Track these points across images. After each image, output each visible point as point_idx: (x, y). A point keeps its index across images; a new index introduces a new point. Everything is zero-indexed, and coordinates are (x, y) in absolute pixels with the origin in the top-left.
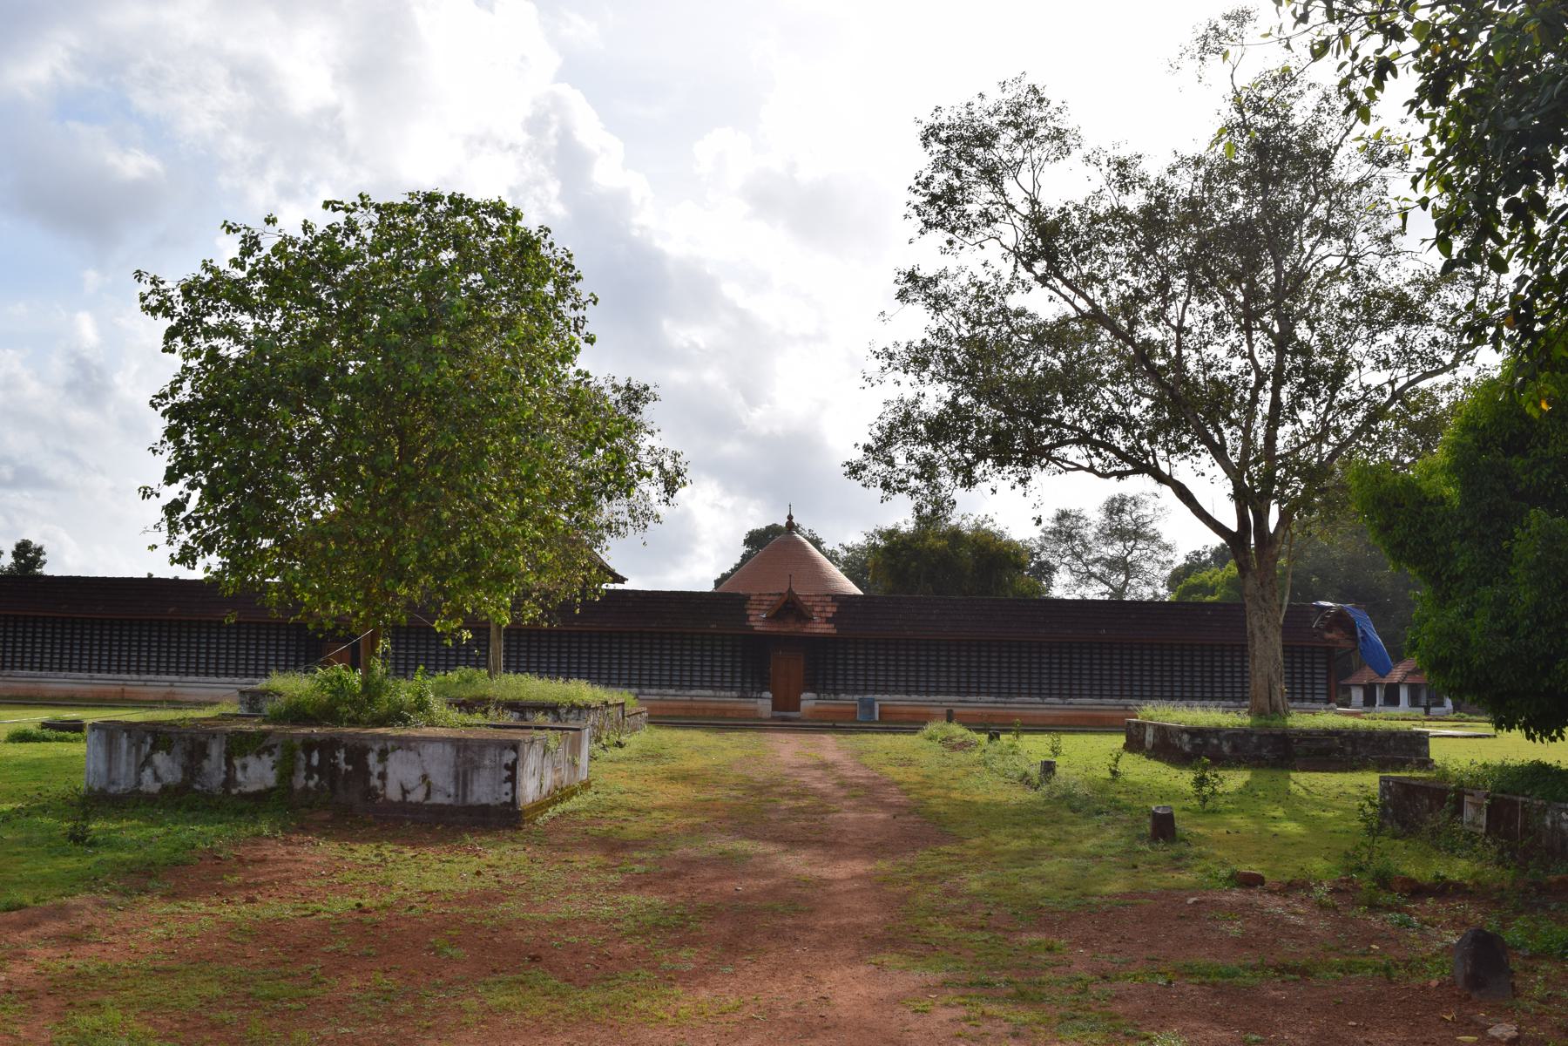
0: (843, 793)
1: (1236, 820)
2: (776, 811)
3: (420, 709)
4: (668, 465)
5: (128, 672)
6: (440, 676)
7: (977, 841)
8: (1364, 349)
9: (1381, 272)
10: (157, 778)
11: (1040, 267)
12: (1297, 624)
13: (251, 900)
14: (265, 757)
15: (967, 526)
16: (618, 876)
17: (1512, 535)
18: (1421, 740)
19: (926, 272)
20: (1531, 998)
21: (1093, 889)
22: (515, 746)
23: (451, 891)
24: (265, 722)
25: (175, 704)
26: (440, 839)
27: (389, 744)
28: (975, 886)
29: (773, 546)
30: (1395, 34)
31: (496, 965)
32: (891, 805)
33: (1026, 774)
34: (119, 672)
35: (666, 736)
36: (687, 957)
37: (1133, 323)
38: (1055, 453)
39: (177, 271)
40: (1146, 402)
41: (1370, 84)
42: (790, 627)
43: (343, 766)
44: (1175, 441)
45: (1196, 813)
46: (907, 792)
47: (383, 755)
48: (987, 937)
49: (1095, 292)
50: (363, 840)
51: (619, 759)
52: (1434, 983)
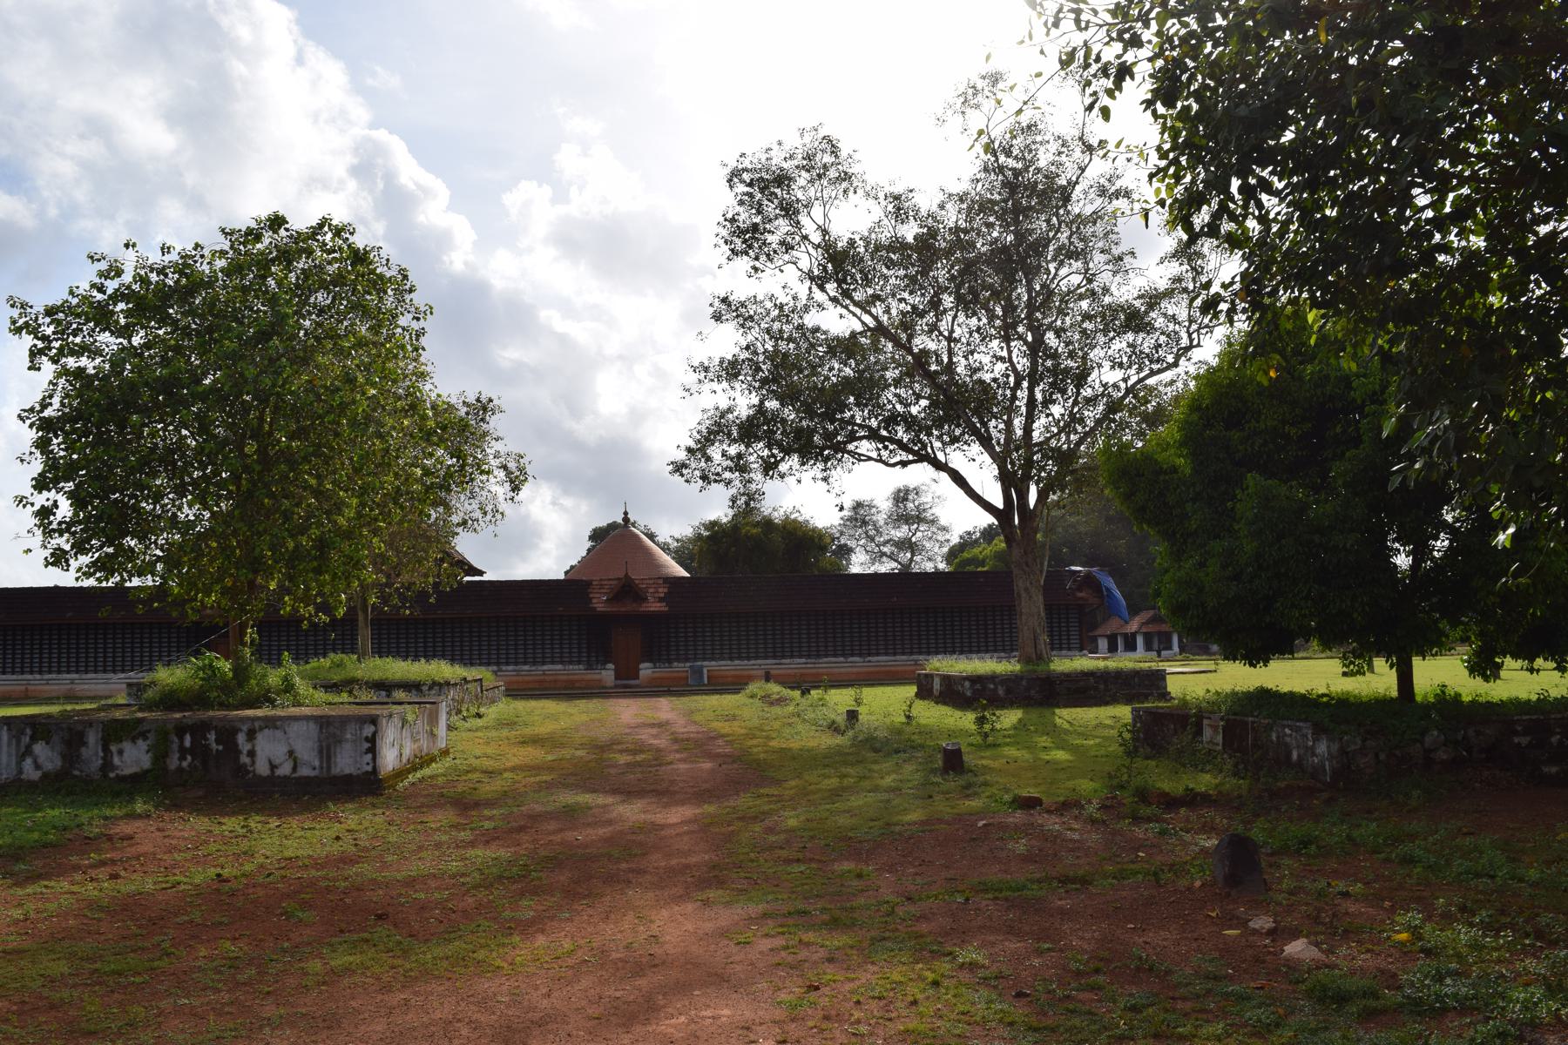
0: (676, 747)
1: (1012, 752)
2: (615, 766)
3: (286, 691)
4: (512, 465)
5: (32, 673)
6: (314, 663)
7: (793, 783)
8: (1102, 354)
9: (1113, 289)
10: (37, 767)
11: (831, 287)
12: (1054, 585)
13: (114, 877)
14: (140, 742)
15: (778, 517)
16: (468, 832)
17: (1235, 496)
18: (1160, 676)
19: (739, 295)
20: (1281, 891)
21: (895, 819)
22: (374, 720)
23: (310, 857)
24: (140, 710)
25: (71, 698)
26: (306, 809)
27: (257, 724)
28: (792, 823)
29: (614, 539)
30: (1136, 42)
31: (343, 926)
32: (718, 755)
33: (834, 722)
34: (22, 673)
35: (521, 706)
36: (528, 908)
37: (910, 337)
38: (851, 447)
39: (44, 296)
40: (924, 403)
41: (1110, 85)
42: (628, 607)
43: (214, 746)
44: (948, 434)
45: (979, 747)
46: (730, 743)
47: (251, 735)
48: (803, 868)
49: (878, 310)
50: (233, 814)
51: (475, 729)
52: (1198, 883)
